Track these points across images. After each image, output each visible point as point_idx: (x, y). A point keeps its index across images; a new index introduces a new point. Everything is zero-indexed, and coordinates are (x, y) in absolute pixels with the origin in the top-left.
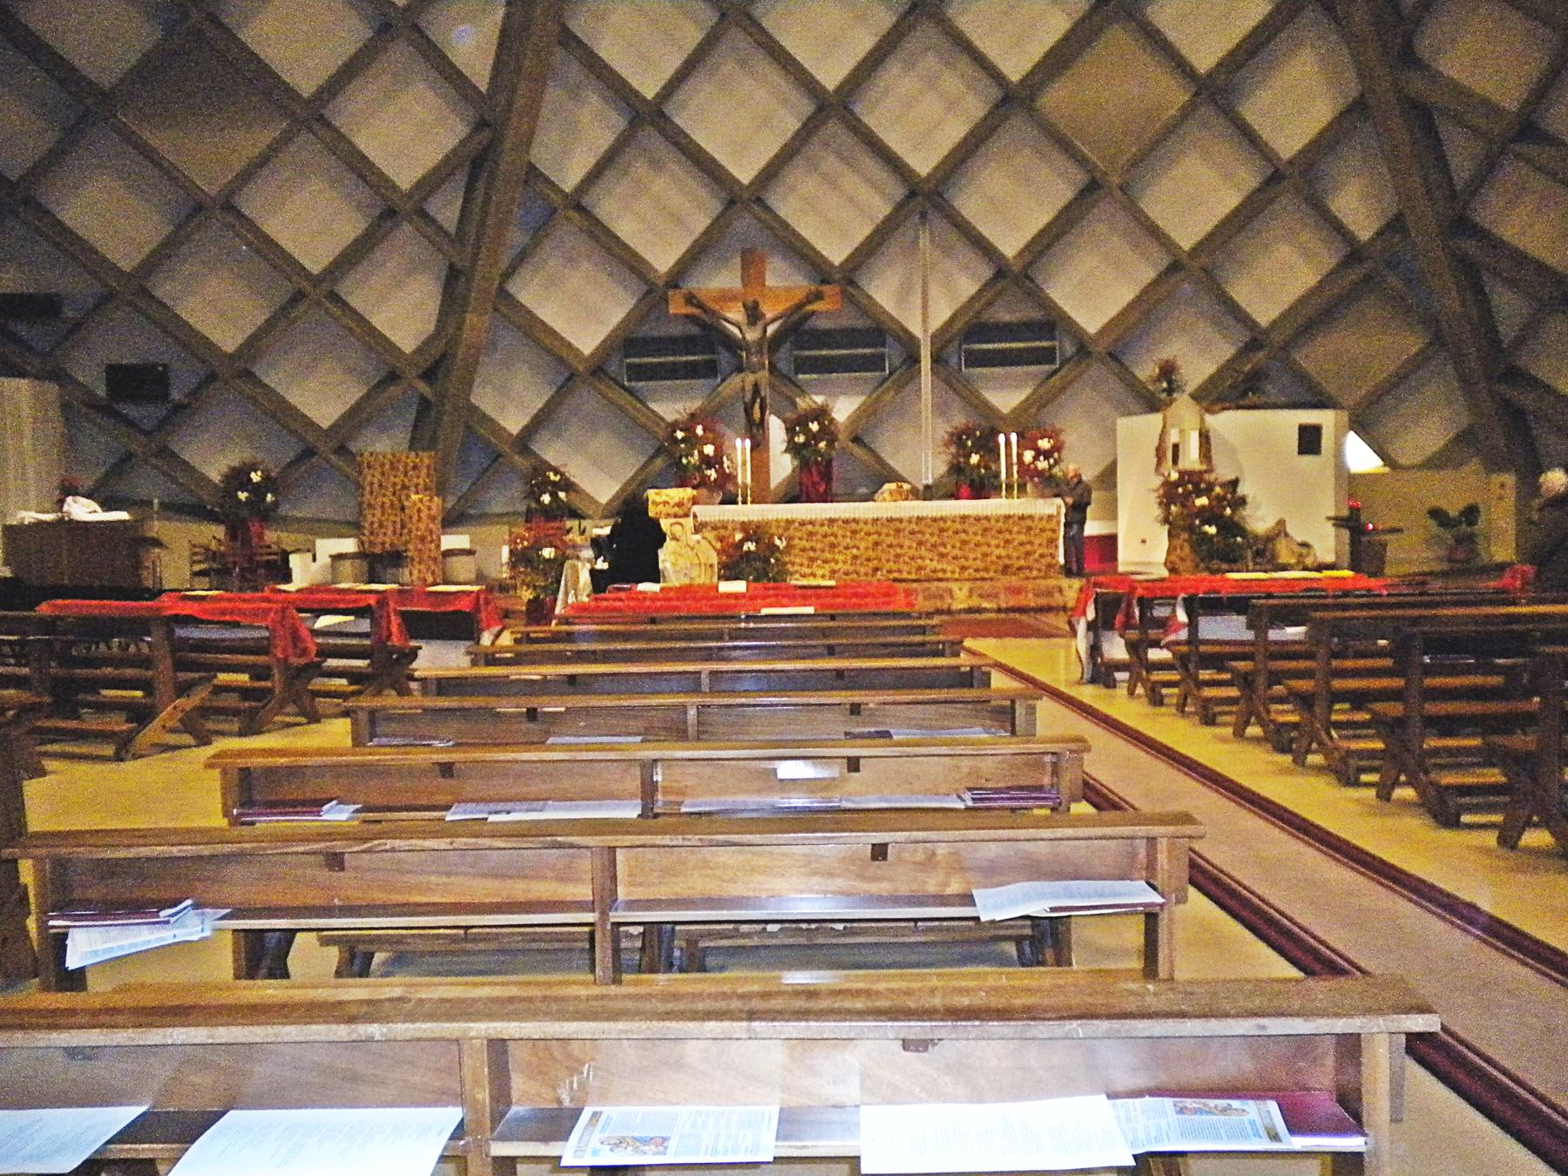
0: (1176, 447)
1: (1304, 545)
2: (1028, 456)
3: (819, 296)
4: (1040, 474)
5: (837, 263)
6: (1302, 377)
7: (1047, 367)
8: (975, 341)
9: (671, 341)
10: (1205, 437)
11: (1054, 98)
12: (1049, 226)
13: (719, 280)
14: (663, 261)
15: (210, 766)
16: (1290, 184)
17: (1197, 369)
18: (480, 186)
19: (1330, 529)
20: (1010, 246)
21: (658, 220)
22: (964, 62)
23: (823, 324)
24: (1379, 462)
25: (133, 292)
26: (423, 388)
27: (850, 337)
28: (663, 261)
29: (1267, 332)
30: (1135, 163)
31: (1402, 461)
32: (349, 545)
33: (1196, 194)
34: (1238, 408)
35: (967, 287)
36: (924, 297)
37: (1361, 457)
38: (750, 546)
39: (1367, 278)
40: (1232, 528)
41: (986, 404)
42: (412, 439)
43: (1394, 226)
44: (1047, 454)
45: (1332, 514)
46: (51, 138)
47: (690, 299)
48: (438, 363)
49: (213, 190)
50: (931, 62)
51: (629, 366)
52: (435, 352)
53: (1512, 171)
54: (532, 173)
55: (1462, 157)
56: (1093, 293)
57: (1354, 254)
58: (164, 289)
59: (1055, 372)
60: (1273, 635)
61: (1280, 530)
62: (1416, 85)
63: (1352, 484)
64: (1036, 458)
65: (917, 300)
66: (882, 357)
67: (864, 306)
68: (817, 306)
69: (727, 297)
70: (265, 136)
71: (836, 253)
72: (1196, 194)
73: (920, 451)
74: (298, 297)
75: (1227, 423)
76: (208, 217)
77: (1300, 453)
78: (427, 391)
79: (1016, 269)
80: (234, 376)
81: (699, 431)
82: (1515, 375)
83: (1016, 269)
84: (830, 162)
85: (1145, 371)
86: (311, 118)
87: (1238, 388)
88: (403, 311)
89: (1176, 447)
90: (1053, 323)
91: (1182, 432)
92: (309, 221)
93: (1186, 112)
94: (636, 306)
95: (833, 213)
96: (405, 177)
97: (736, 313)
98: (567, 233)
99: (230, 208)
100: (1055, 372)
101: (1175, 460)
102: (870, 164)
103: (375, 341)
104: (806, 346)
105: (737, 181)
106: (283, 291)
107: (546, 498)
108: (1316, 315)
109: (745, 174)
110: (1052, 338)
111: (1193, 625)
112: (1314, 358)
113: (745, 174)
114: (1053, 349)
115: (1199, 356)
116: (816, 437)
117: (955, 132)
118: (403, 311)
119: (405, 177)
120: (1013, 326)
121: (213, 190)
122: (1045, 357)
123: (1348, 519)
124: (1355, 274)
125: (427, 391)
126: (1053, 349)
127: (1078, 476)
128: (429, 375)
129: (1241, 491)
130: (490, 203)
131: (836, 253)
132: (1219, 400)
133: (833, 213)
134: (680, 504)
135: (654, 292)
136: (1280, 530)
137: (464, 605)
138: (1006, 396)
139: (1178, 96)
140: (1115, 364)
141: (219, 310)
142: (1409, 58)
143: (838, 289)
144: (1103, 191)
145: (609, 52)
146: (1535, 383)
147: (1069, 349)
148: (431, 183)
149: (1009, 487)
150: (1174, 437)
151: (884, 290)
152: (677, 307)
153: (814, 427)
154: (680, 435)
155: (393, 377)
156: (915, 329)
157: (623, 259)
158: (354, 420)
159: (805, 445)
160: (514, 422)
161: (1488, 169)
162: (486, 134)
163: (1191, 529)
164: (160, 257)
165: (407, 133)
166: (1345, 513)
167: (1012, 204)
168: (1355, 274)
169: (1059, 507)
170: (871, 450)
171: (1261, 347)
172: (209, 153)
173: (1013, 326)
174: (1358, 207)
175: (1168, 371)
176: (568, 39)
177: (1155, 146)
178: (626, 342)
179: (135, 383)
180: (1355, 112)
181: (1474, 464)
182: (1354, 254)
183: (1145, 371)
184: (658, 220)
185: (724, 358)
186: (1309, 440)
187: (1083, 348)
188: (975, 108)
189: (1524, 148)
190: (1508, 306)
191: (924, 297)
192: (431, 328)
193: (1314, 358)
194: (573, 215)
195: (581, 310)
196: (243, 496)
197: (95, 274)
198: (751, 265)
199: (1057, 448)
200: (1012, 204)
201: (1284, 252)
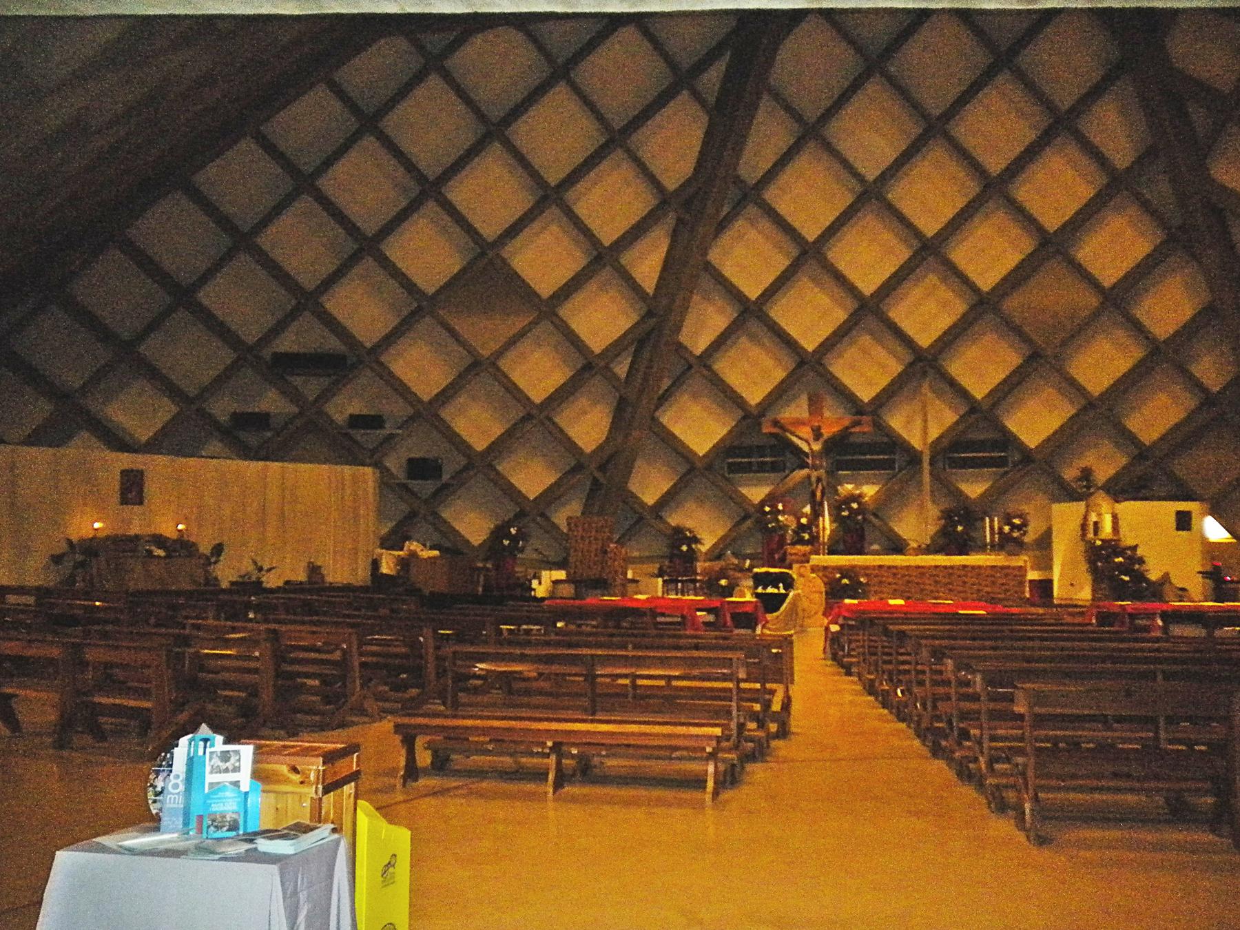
1: (1183, 589)
2: (1007, 528)
3: (858, 423)
4: (1015, 539)
5: (866, 401)
6: (1172, 477)
7: (1002, 470)
8: (954, 452)
9: (756, 445)
10: (1115, 518)
11: (1012, 304)
13: (796, 410)
14: (754, 397)
16: (1162, 358)
17: (1103, 473)
18: (646, 355)
19: (1200, 578)
20: (979, 391)
21: (753, 374)
23: (859, 440)
24: (1228, 535)
25: (428, 414)
26: (598, 475)
27: (871, 448)
28: (754, 397)
29: (1150, 448)
30: (1064, 343)
32: (561, 575)
33: (1101, 363)
34: (1135, 499)
35: (950, 418)
36: (921, 424)
37: (1214, 531)
38: (845, 581)
40: (1140, 577)
41: (961, 492)
44: (1019, 528)
45: (1201, 569)
46: (394, 322)
47: (776, 423)
48: (611, 458)
49: (485, 353)
50: (932, 279)
51: (730, 465)
54: (680, 346)
56: (1034, 422)
57: (1208, 399)
58: (446, 413)
59: (1006, 473)
60: (1217, 633)
61: (1166, 578)
63: (1211, 550)
64: (1011, 530)
65: (919, 422)
66: (894, 461)
67: (880, 426)
68: (857, 429)
69: (799, 423)
70: (520, 323)
71: (865, 394)
73: (915, 523)
74: (528, 417)
75: (1131, 510)
76: (478, 370)
77: (1189, 529)
78: (600, 477)
79: (985, 407)
80: (482, 466)
81: (780, 507)
83: (985, 407)
84: (866, 340)
85: (1070, 474)
86: (547, 311)
87: (1128, 487)
88: (588, 427)
89: (1096, 523)
90: (1008, 440)
91: (1099, 515)
93: (1096, 314)
94: (736, 426)
95: (866, 371)
96: (597, 345)
97: (806, 432)
98: (696, 381)
99: (494, 364)
101: (1096, 533)
102: (892, 342)
103: (571, 446)
104: (844, 453)
105: (806, 350)
106: (517, 413)
107: (684, 548)
108: (1182, 438)
109: (810, 346)
111: (1165, 629)
112: (1182, 467)
113: (810, 346)
115: (1105, 462)
116: (857, 512)
117: (944, 322)
118: (588, 427)
119: (597, 345)
120: (979, 438)
121: (485, 353)
122: (1001, 463)
123: (1211, 573)
125: (600, 477)
128: (602, 468)
129: (1139, 552)
130: (652, 363)
131: (865, 394)
132: (1123, 491)
133: (866, 371)
134: (804, 555)
135: (750, 418)
136: (1166, 578)
137: (749, 609)
138: (974, 489)
139: (1093, 301)
140: (1044, 469)
141: (477, 424)
143: (870, 418)
144: (1040, 362)
145: (729, 272)
148: (615, 349)
149: (993, 546)
150: (1093, 517)
151: (898, 421)
152: (767, 429)
153: (855, 506)
154: (767, 509)
155: (578, 468)
156: (916, 443)
157: (730, 397)
158: (551, 496)
159: (848, 517)
160: (650, 499)
163: (1112, 578)
165: (602, 320)
166: (1208, 568)
167: (981, 368)
169: (1025, 562)
170: (882, 520)
171: (1147, 458)
172: (485, 333)
173: (979, 438)
175: (1087, 474)
176: (709, 268)
177: (1078, 331)
178: (725, 449)
179: (421, 468)
182: (1208, 399)
183: (1070, 474)
184: (753, 374)
185: (790, 459)
186: (1184, 521)
188: (960, 307)
191: (921, 424)
193: (1182, 467)
194: (699, 371)
195: (699, 428)
196: (506, 542)
197: (411, 403)
198: (815, 404)
199: (1025, 524)
200: (981, 368)
201: (1163, 398)
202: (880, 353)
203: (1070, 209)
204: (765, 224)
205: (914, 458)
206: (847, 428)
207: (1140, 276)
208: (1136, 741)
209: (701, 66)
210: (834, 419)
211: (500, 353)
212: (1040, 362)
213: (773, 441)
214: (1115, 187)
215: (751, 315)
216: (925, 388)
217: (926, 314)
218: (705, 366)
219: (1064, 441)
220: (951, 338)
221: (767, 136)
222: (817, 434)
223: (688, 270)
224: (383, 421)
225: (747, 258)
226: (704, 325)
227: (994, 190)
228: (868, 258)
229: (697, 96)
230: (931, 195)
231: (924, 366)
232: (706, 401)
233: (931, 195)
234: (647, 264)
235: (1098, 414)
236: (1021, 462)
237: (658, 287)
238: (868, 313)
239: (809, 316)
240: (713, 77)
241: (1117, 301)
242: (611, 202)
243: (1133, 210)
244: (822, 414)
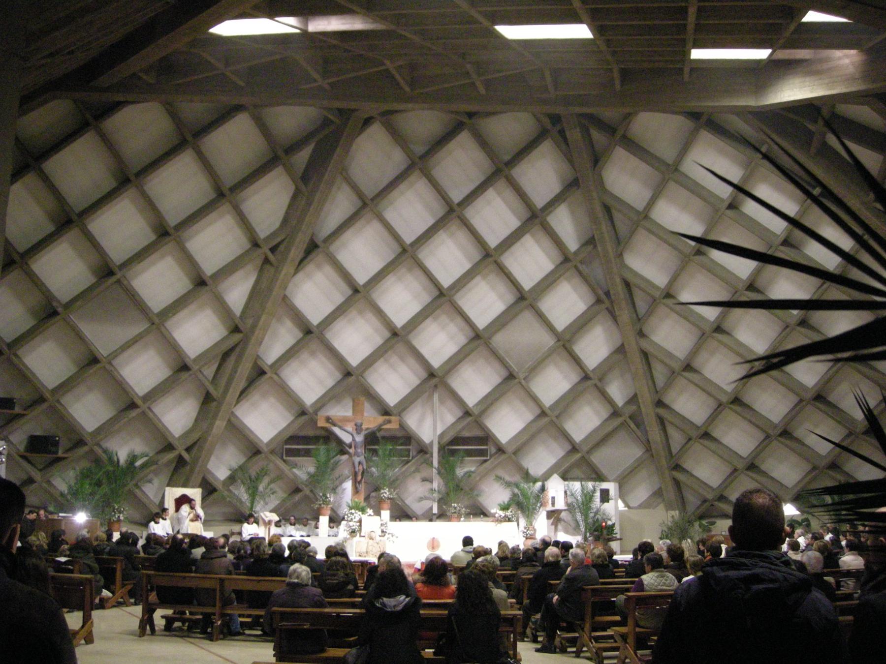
0: (553, 498)
9: (310, 437)
12: (489, 394)
15: (163, 617)
21: (309, 380)
22: (459, 320)
31: (631, 505)
33: (553, 384)
36: (430, 425)
39: (622, 424)
42: (171, 479)
43: (633, 400)
52: (195, 436)
53: (681, 382)
55: (660, 374)
56: (507, 424)
62: (644, 344)
66: (409, 451)
69: (346, 420)
72: (553, 384)
82: (677, 467)
86: (157, 324)
90: (486, 438)
92: (142, 371)
97: (350, 427)
100: (486, 461)
108: (600, 439)
110: (487, 445)
112: (598, 458)
114: (487, 450)
124: (617, 422)
126: (487, 450)
127: (157, 523)
130: (236, 369)
133: (393, 382)
139: (549, 341)
142: (641, 334)
144: (513, 381)
146: (685, 471)
147: (493, 450)
161: (669, 384)
162: (237, 337)
164: (66, 386)
165: (197, 332)
167: (475, 383)
168: (617, 422)
173: (471, 441)
174: (618, 392)
180: (621, 350)
181: (662, 506)
182: (615, 413)
184: (309, 380)
187: (500, 450)
189: (686, 374)
190: (677, 439)
191: (430, 425)
192: (191, 425)
195: (264, 420)
202: (404, 369)
203: (539, 276)
204: (547, 242)
205: (423, 450)
206: (381, 425)
207: (581, 325)
208: (249, 616)
209: (292, 148)
210: (371, 419)
211: (115, 354)
212: (513, 381)
213: (323, 433)
214: (567, 263)
215: (312, 335)
216: (436, 397)
217: (439, 342)
218: (276, 374)
219: (526, 440)
220: (455, 362)
221: (339, 205)
222: (358, 428)
223: (267, 298)
224: (14, 403)
225: (313, 293)
226: (277, 341)
227: (490, 259)
228: (401, 299)
229: (289, 170)
230: (448, 258)
231: (435, 381)
232: (272, 400)
233: (448, 258)
234: (237, 292)
235: (548, 421)
236: (496, 453)
237: (244, 312)
238: (398, 339)
239: (355, 339)
240: (303, 156)
241: (565, 343)
242: (215, 242)
243: (577, 280)
244: (362, 415)
